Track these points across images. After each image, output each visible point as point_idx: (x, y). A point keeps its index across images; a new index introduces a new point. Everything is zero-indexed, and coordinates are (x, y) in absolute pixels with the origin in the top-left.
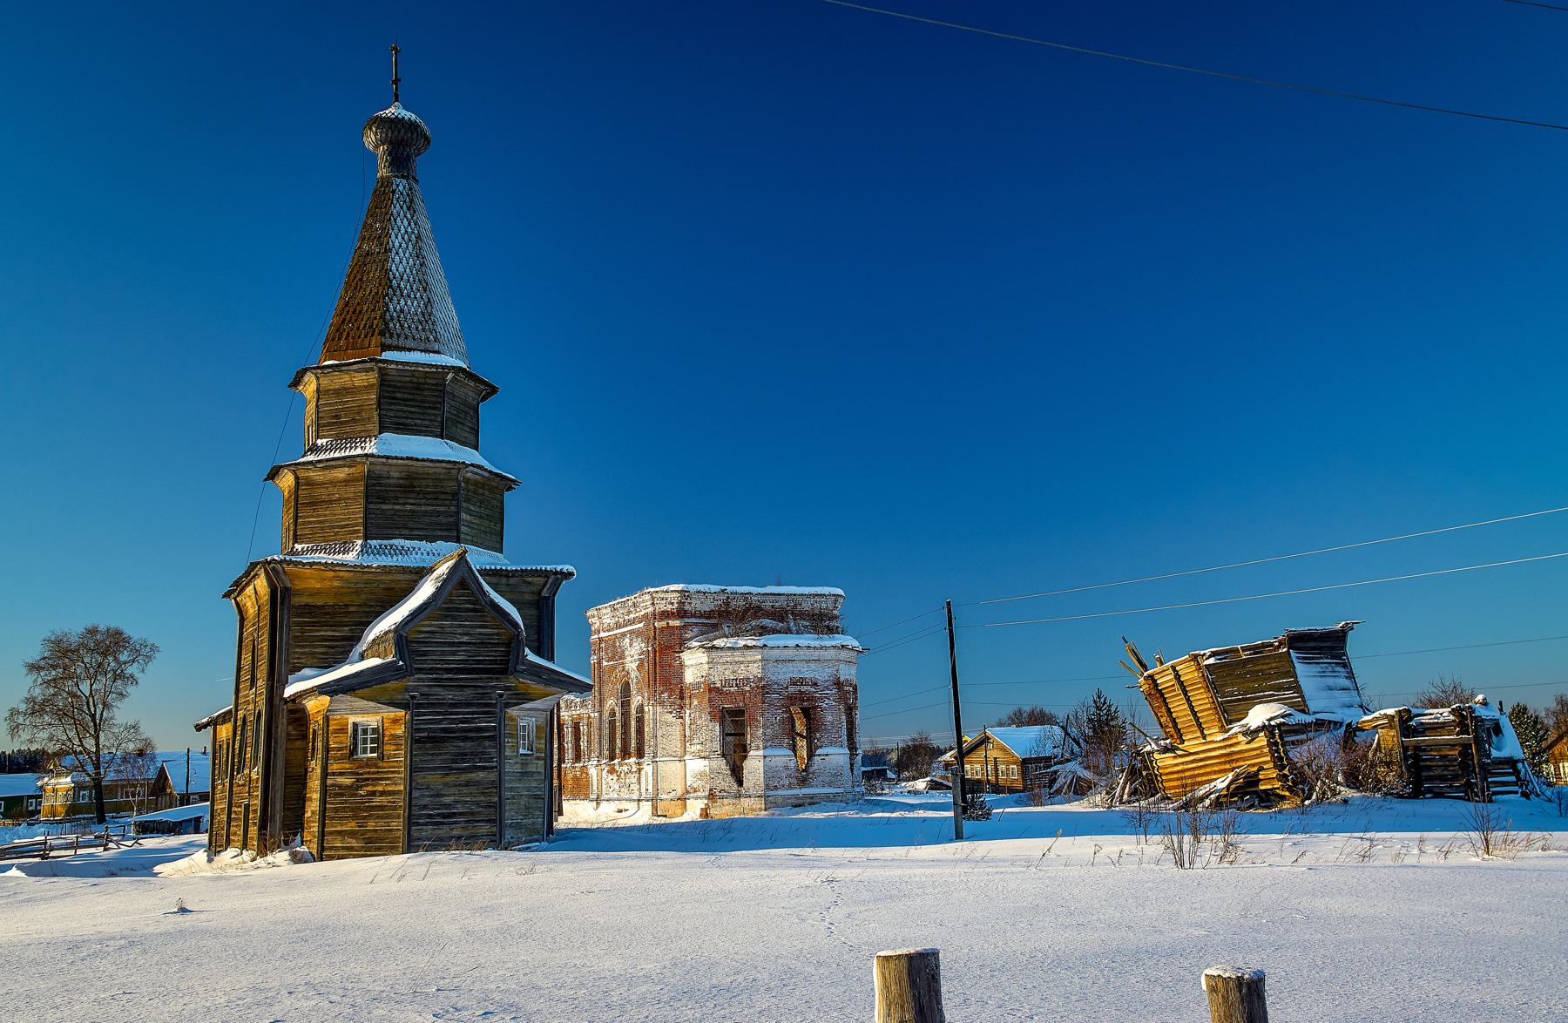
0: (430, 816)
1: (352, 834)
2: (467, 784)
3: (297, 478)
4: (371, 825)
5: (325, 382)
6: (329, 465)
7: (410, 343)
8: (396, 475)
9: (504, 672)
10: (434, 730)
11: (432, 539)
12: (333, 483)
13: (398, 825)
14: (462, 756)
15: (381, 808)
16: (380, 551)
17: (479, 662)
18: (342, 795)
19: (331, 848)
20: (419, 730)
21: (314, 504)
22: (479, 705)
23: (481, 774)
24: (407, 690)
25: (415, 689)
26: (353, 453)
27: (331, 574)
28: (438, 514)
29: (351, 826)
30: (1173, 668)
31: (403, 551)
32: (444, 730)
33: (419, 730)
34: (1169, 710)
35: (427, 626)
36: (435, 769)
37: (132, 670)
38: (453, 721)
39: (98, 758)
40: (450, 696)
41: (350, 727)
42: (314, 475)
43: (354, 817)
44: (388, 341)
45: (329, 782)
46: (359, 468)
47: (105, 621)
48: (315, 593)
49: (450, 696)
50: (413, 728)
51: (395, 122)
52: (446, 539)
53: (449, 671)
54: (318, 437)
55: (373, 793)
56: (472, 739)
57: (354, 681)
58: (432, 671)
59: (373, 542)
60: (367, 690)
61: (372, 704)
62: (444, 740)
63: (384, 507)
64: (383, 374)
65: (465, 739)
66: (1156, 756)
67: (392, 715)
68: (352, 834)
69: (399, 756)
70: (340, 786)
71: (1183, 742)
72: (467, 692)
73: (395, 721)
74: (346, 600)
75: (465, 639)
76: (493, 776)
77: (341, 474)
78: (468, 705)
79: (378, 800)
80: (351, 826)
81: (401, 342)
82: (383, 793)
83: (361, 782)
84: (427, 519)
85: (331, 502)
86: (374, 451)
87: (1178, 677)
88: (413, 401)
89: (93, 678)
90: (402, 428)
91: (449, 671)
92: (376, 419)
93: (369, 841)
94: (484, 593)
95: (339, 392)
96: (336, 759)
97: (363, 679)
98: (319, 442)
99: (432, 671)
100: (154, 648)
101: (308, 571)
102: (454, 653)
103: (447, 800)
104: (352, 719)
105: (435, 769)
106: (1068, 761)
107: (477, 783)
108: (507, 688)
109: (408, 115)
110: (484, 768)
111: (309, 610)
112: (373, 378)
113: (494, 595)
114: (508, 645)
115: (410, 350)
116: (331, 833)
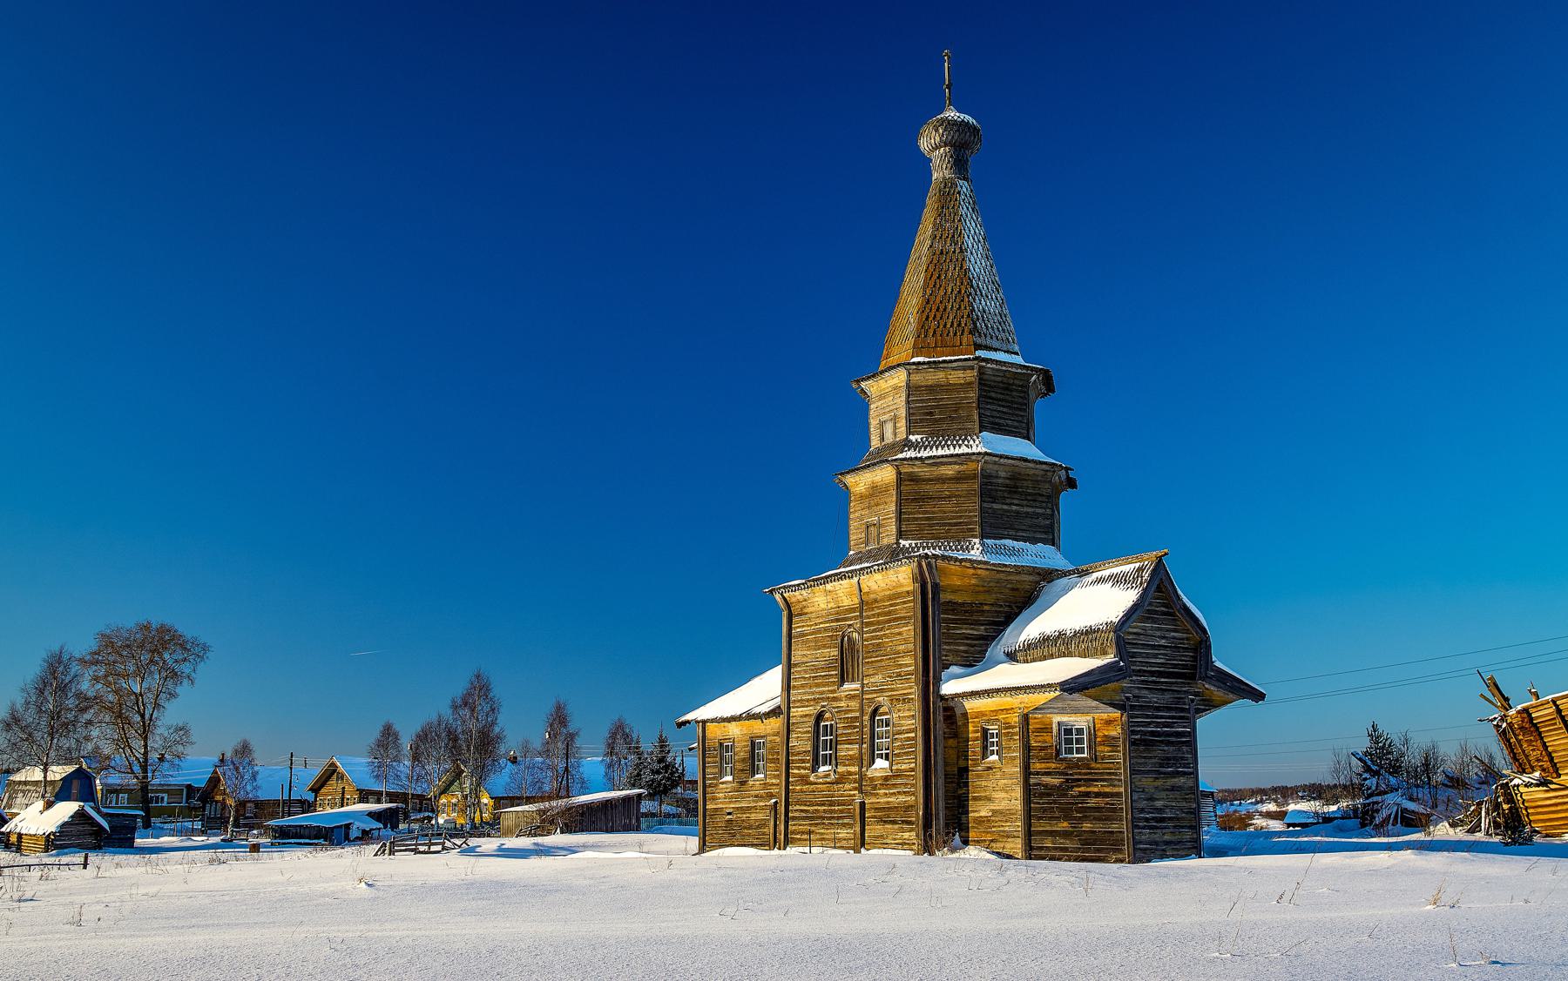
0: (1147, 820)
1: (1065, 834)
2: (1173, 789)
3: (899, 473)
4: (1087, 826)
5: (916, 378)
6: (937, 461)
7: (996, 344)
8: (1002, 474)
9: (1192, 677)
10: (1145, 733)
11: (1034, 541)
12: (942, 480)
13: (1122, 826)
14: (1166, 761)
15: (1098, 809)
16: (997, 551)
17: (1175, 666)
18: (1049, 795)
19: (1041, 848)
20: (1133, 732)
21: (921, 499)
22: (1176, 709)
23: (1182, 780)
24: (1123, 691)
25: (1129, 690)
26: (958, 451)
27: (971, 571)
28: (1037, 515)
29: (1064, 825)
30: (1554, 701)
31: (1013, 552)
32: (1153, 733)
33: (1133, 732)
34: (1544, 744)
35: (1135, 626)
36: (1149, 772)
37: (186, 668)
38: (1158, 725)
39: (146, 760)
40: (1154, 698)
41: (1055, 727)
42: (917, 469)
43: (1066, 818)
44: (979, 341)
45: (1032, 781)
46: (972, 466)
47: (158, 618)
48: (955, 591)
49: (1154, 698)
50: (1130, 730)
51: (950, 124)
52: (1045, 542)
53: (1152, 673)
54: (909, 432)
55: (1087, 794)
56: (1172, 743)
57: (1087, 679)
58: (1140, 673)
59: (989, 541)
60: (1092, 691)
61: (1095, 703)
62: (1153, 743)
63: (995, 506)
64: (981, 371)
65: (1169, 743)
66: (1522, 789)
67: (1105, 716)
68: (1065, 834)
69: (1120, 759)
70: (1046, 786)
71: (1559, 776)
72: (1167, 696)
73: (1109, 722)
74: (981, 598)
75: (1163, 642)
76: (1190, 783)
77: (949, 471)
78: (1169, 709)
79: (1092, 802)
80: (1064, 825)
81: (989, 342)
82: (1098, 795)
83: (1071, 783)
84: (1028, 521)
85: (940, 498)
86: (980, 449)
87: (1559, 711)
88: (1005, 401)
89: (141, 673)
90: (998, 428)
91: (1152, 673)
92: (976, 417)
93: (1085, 842)
94: (1178, 596)
95: (931, 389)
96: (1041, 760)
97: (1092, 678)
98: (912, 438)
99: (1140, 673)
100: (205, 648)
101: (953, 567)
102: (1155, 656)
103: (1159, 804)
104: (1056, 719)
105: (1149, 772)
106: (1385, 793)
107: (1179, 789)
108: (1196, 694)
109: (971, 120)
110: (1184, 774)
111: (952, 607)
112: (971, 375)
113: (1185, 599)
114: (1195, 650)
115: (996, 350)
116: (1041, 833)
